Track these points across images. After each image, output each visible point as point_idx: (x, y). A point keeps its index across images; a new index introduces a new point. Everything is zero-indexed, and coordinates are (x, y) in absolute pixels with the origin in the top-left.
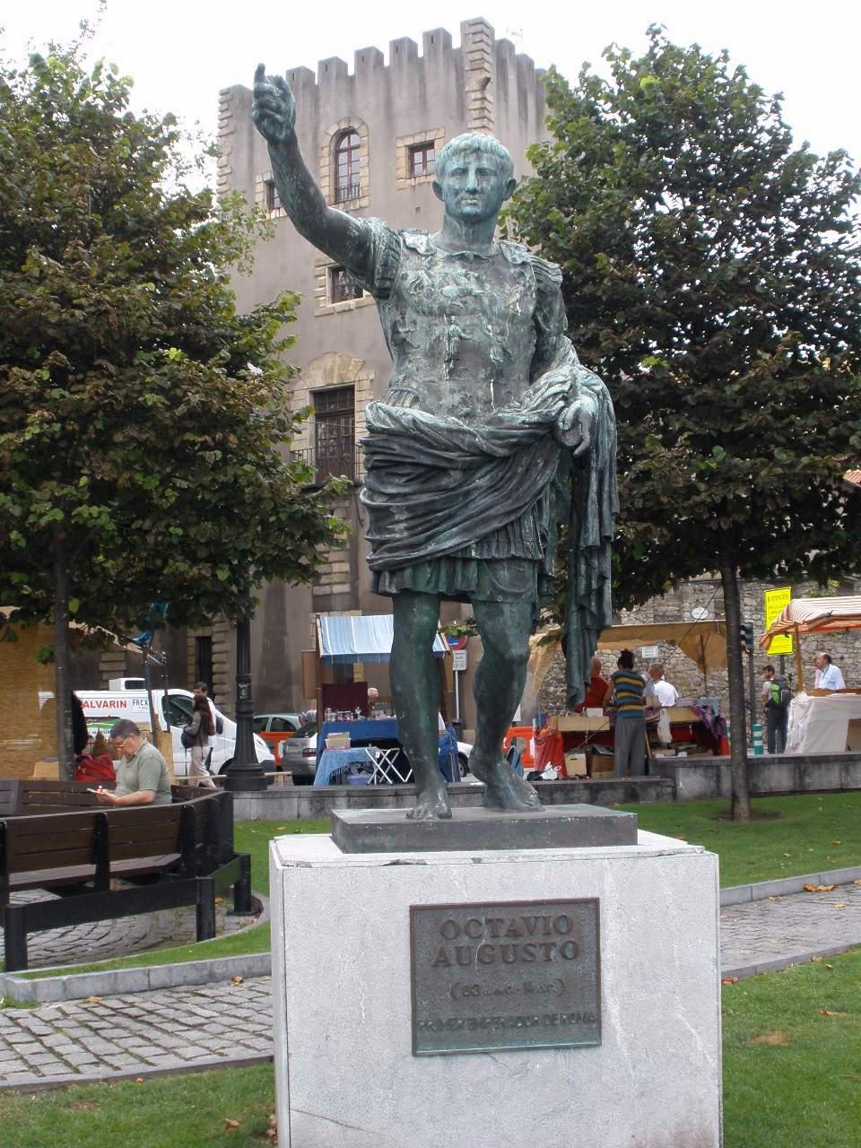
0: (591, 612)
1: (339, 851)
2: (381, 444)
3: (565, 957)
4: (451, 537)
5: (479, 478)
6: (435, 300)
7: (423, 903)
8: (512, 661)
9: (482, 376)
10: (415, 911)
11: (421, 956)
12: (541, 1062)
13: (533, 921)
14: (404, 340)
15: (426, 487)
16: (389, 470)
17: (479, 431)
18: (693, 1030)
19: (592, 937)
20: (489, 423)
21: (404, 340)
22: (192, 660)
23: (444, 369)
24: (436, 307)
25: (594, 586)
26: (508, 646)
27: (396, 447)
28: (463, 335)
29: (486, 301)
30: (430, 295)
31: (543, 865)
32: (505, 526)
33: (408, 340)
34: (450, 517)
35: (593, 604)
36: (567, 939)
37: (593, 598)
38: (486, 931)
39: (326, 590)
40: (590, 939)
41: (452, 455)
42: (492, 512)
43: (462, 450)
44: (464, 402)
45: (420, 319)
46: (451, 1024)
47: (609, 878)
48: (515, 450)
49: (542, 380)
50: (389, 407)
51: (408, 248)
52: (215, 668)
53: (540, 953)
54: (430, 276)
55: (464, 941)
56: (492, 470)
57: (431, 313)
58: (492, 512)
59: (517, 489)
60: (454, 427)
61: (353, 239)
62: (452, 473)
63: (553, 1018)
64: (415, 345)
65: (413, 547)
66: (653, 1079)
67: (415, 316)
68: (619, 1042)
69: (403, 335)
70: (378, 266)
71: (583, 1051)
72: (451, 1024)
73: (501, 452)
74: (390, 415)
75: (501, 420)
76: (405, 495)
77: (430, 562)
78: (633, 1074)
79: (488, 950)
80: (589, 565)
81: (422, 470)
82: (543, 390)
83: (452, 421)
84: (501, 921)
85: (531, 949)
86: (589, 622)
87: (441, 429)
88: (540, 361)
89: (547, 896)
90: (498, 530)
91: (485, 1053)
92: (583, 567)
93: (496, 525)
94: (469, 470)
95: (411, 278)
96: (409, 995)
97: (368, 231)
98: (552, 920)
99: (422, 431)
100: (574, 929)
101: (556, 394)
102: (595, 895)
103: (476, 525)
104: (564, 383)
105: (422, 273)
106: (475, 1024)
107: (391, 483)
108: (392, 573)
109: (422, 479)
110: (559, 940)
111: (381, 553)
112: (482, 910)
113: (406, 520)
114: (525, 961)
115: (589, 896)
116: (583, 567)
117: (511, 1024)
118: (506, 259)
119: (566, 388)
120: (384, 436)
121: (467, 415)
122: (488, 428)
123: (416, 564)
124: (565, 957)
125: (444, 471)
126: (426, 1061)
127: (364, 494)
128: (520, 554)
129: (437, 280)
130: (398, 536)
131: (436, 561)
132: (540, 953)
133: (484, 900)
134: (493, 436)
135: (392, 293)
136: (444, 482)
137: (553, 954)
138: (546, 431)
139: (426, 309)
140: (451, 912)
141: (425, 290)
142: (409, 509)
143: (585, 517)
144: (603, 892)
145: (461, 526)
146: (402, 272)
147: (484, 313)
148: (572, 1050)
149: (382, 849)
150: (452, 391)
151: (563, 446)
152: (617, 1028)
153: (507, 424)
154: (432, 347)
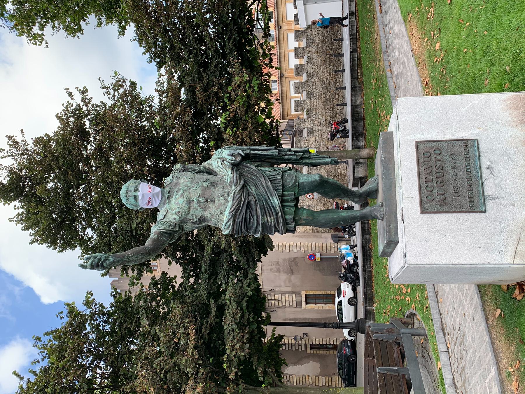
0: (303, 155)
1: (399, 244)
2: (238, 227)
6: (184, 207)
7: (419, 208)
8: (320, 180)
10: (423, 211)
12: (485, 162)
13: (426, 166)
15: (255, 209)
16: (248, 224)
17: (234, 189)
18: (470, 105)
20: (231, 186)
21: (199, 219)
22: (318, 352)
23: (211, 205)
24: (187, 206)
28: (198, 196)
29: (186, 188)
30: (182, 208)
31: (402, 162)
32: (270, 181)
33: (199, 217)
34: (266, 200)
35: (300, 154)
37: (298, 154)
38: (430, 184)
39: (295, 303)
41: (243, 199)
42: (264, 185)
44: (223, 196)
45: (191, 213)
47: (407, 138)
48: (242, 177)
50: (224, 224)
51: (164, 219)
52: (321, 343)
53: (439, 163)
54: (175, 209)
55: (435, 192)
56: (249, 186)
57: (189, 208)
58: (264, 185)
60: (232, 198)
61: (158, 237)
62: (249, 200)
63: (466, 158)
64: (201, 215)
65: (277, 215)
66: (491, 119)
67: (190, 215)
68: (476, 133)
69: (197, 220)
70: (170, 229)
73: (242, 182)
74: (227, 223)
75: (230, 182)
76: (257, 217)
77: (283, 209)
78: (489, 127)
79: (438, 183)
81: (248, 210)
83: (230, 199)
85: (437, 167)
86: (307, 156)
87: (233, 203)
88: (210, 172)
90: (272, 183)
91: (482, 184)
92: (286, 157)
93: (269, 184)
94: (248, 194)
95: (175, 216)
96: (459, 214)
97: (156, 232)
98: (425, 159)
99: (233, 210)
100: (429, 150)
102: (414, 143)
103: (269, 191)
104: (217, 161)
105: (174, 212)
106: (470, 186)
107: (253, 223)
108: (287, 224)
109: (251, 210)
110: (433, 156)
111: (279, 228)
112: (421, 185)
113: (267, 217)
116: (286, 157)
117: (469, 173)
118: (170, 183)
121: (228, 195)
122: (233, 186)
123: (284, 213)
125: (249, 203)
126: (487, 207)
127: (257, 235)
129: (176, 206)
130: (273, 221)
131: (283, 206)
132: (439, 163)
133: (417, 177)
134: (236, 184)
135: (181, 224)
136: (253, 203)
137: (439, 157)
138: (235, 166)
139: (187, 210)
141: (180, 210)
142: (263, 216)
143: (268, 155)
144: (413, 140)
145: (270, 196)
146: (173, 220)
148: (480, 150)
149: (396, 228)
150: (219, 200)
151: (241, 161)
153: (232, 179)
154: (202, 208)
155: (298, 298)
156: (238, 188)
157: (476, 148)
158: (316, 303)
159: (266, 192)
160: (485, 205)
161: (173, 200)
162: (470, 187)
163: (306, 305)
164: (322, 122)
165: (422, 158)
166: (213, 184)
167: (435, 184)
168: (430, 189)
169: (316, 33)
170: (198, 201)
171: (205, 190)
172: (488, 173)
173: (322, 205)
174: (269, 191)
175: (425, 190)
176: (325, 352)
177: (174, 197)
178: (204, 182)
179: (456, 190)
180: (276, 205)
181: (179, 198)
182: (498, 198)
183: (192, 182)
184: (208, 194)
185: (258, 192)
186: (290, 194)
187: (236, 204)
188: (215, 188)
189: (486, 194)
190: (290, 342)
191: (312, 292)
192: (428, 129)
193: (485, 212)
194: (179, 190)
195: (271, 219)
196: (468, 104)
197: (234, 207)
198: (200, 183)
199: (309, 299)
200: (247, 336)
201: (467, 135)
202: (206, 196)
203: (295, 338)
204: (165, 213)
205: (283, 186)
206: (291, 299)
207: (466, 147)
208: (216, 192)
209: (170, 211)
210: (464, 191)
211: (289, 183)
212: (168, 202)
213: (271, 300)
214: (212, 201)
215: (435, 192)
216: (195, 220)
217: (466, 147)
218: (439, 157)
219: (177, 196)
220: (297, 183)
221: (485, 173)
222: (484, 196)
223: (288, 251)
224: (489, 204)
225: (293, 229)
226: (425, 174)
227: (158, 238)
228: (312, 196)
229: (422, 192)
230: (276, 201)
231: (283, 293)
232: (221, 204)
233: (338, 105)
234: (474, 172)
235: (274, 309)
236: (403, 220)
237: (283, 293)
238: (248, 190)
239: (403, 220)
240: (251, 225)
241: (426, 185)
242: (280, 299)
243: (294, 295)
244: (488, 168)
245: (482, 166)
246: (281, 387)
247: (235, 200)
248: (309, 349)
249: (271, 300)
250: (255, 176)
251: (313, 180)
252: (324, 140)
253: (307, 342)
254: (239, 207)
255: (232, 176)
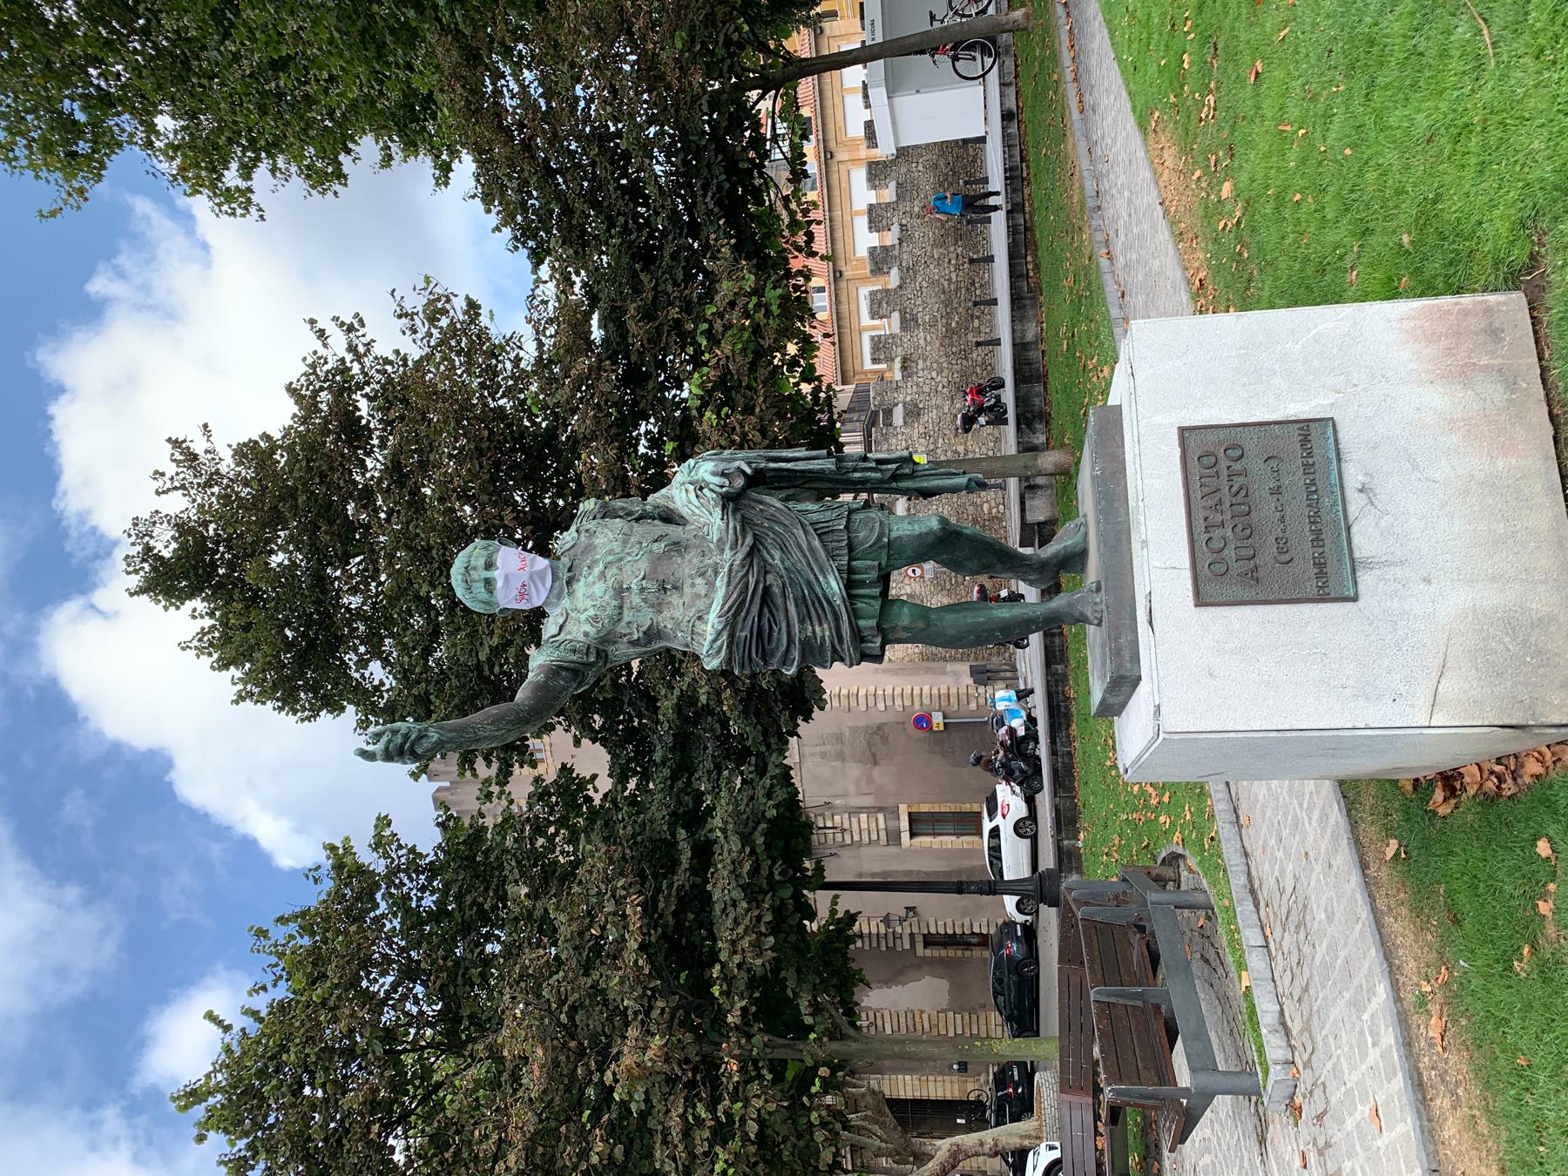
0: (897, 469)
1: (1142, 684)
3: (1241, 457)
4: (828, 583)
5: (773, 559)
7: (1191, 594)
8: (943, 529)
9: (679, 560)
10: (1201, 601)
11: (1247, 596)
12: (1353, 476)
13: (1206, 490)
14: (645, 633)
17: (729, 558)
18: (1313, 332)
19: (1222, 434)
20: (722, 551)
21: (645, 633)
22: (943, 953)
23: (674, 598)
25: (873, 465)
26: (931, 532)
27: (743, 634)
29: (610, 558)
31: (1146, 481)
32: (819, 535)
33: (645, 628)
34: (809, 584)
36: (1222, 455)
37: (884, 467)
39: (883, 834)
40: (1222, 434)
42: (805, 546)
43: (748, 572)
44: (702, 575)
46: (1320, 566)
47: (1158, 419)
49: (685, 512)
50: (706, 644)
52: (950, 931)
53: (1238, 481)
55: (1230, 553)
57: (621, 607)
58: (805, 546)
59: (785, 525)
60: (726, 579)
61: (547, 677)
63: (1306, 466)
65: (837, 618)
67: (623, 624)
69: (641, 635)
71: (1340, 435)
72: (1320, 566)
74: (714, 641)
75: (720, 540)
77: (851, 604)
79: (1238, 530)
80: (855, 470)
82: (693, 508)
83: (721, 583)
84: (1206, 519)
85: (1234, 490)
86: (907, 471)
87: (727, 592)
88: (669, 517)
89: (1179, 477)
90: (822, 541)
91: (1348, 529)
92: (857, 475)
93: (817, 543)
94: (765, 570)
95: (587, 628)
97: (540, 666)
98: (1203, 471)
101: (697, 497)
102: (1175, 431)
103: (816, 560)
105: (583, 617)
106: (1317, 540)
107: (778, 639)
108: (863, 640)
110: (1224, 464)
111: (843, 650)
112: (1195, 537)
113: (812, 625)
114: (1246, 496)
115: (1175, 437)
116: (857, 475)
119: (691, 488)
120: (734, 648)
121: (716, 573)
122: (727, 551)
123: (855, 615)
124: (1241, 457)
125: (767, 590)
126: (1361, 587)
128: (844, 522)
129: (589, 603)
130: (827, 633)
131: (851, 598)
132: (1238, 481)
136: (776, 590)
137: (1237, 466)
138: (731, 501)
139: (616, 612)
140: (1199, 567)
142: (801, 622)
143: (810, 471)
146: (581, 638)
147: (621, 559)
149: (1135, 643)
150: (693, 585)
152: (1314, 404)
153: (724, 532)
154: (652, 606)
155: (892, 824)
156: (740, 556)
157: (1332, 440)
158: (935, 834)
159: (809, 564)
160: (1356, 583)
161: (580, 587)
162: (1317, 539)
163: (911, 838)
164: (940, 388)
165: (1195, 469)
166: (677, 547)
167: (1229, 533)
168: (1216, 545)
169: (920, 168)
170: (642, 590)
171: (657, 561)
172: (1363, 504)
173: (945, 592)
174: (816, 560)
175: (1205, 548)
176: (959, 953)
177: (582, 579)
178: (656, 541)
179: (1283, 545)
180: (834, 594)
181: (594, 583)
182: (1391, 564)
183: (625, 542)
184: (665, 571)
185: (787, 563)
186: (867, 568)
187: (735, 595)
188: (683, 557)
189: (1357, 554)
190: (874, 931)
191: (925, 808)
192: (1210, 398)
193: (1355, 599)
194: (595, 562)
195: (823, 631)
196: (1309, 330)
197: (731, 601)
198: (645, 545)
199: (918, 824)
200: (768, 917)
201: (1307, 408)
202: (661, 577)
203: (887, 920)
204: (561, 621)
205: (851, 548)
206: (873, 826)
207: (1305, 440)
208: (685, 567)
209: (573, 615)
210: (1303, 550)
211: (866, 539)
212: (570, 594)
213: (825, 828)
214: (675, 588)
215: (1230, 553)
216: (636, 637)
217: (1305, 440)
218: (1237, 466)
219: (591, 579)
220: (886, 540)
221: (1355, 503)
222: (1352, 560)
223: (863, 708)
224: (1366, 579)
225: (877, 652)
226: (1204, 507)
227: (545, 682)
228: (918, 572)
229: (1198, 554)
230: (834, 584)
231: (854, 812)
232: (698, 596)
233: (978, 344)
234: (1326, 502)
235: (833, 851)
236: (1151, 623)
237: (854, 812)
238: (764, 560)
239: (1151, 623)
240: (774, 645)
241: (1208, 535)
242: (846, 825)
243: (881, 816)
244: (1361, 491)
245: (1345, 485)
246: (856, 1040)
247: (734, 584)
248: (920, 946)
249: (825, 828)
250: (781, 523)
251: (924, 530)
252: (947, 432)
253: (916, 930)
254: (744, 601)
255: (723, 526)
